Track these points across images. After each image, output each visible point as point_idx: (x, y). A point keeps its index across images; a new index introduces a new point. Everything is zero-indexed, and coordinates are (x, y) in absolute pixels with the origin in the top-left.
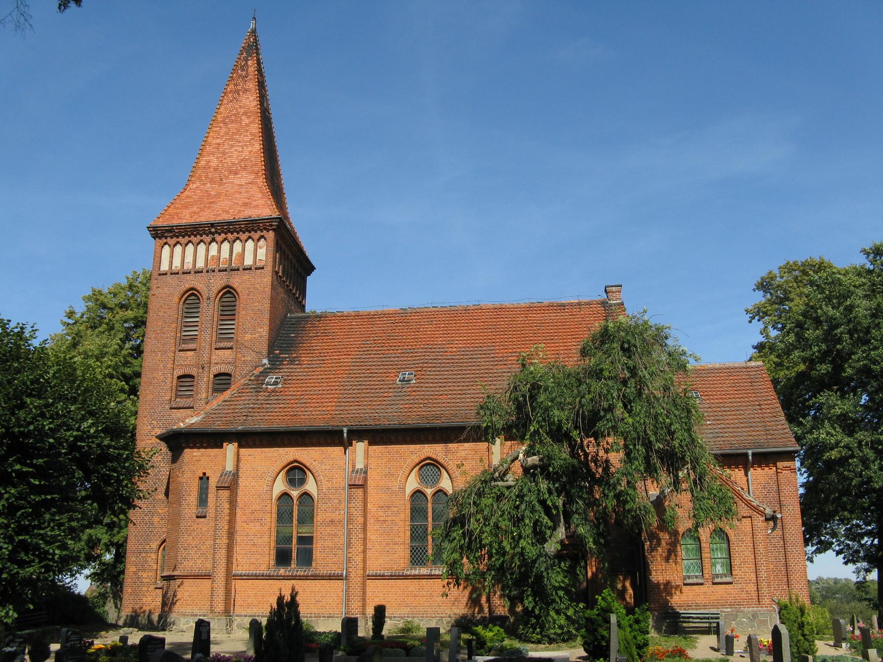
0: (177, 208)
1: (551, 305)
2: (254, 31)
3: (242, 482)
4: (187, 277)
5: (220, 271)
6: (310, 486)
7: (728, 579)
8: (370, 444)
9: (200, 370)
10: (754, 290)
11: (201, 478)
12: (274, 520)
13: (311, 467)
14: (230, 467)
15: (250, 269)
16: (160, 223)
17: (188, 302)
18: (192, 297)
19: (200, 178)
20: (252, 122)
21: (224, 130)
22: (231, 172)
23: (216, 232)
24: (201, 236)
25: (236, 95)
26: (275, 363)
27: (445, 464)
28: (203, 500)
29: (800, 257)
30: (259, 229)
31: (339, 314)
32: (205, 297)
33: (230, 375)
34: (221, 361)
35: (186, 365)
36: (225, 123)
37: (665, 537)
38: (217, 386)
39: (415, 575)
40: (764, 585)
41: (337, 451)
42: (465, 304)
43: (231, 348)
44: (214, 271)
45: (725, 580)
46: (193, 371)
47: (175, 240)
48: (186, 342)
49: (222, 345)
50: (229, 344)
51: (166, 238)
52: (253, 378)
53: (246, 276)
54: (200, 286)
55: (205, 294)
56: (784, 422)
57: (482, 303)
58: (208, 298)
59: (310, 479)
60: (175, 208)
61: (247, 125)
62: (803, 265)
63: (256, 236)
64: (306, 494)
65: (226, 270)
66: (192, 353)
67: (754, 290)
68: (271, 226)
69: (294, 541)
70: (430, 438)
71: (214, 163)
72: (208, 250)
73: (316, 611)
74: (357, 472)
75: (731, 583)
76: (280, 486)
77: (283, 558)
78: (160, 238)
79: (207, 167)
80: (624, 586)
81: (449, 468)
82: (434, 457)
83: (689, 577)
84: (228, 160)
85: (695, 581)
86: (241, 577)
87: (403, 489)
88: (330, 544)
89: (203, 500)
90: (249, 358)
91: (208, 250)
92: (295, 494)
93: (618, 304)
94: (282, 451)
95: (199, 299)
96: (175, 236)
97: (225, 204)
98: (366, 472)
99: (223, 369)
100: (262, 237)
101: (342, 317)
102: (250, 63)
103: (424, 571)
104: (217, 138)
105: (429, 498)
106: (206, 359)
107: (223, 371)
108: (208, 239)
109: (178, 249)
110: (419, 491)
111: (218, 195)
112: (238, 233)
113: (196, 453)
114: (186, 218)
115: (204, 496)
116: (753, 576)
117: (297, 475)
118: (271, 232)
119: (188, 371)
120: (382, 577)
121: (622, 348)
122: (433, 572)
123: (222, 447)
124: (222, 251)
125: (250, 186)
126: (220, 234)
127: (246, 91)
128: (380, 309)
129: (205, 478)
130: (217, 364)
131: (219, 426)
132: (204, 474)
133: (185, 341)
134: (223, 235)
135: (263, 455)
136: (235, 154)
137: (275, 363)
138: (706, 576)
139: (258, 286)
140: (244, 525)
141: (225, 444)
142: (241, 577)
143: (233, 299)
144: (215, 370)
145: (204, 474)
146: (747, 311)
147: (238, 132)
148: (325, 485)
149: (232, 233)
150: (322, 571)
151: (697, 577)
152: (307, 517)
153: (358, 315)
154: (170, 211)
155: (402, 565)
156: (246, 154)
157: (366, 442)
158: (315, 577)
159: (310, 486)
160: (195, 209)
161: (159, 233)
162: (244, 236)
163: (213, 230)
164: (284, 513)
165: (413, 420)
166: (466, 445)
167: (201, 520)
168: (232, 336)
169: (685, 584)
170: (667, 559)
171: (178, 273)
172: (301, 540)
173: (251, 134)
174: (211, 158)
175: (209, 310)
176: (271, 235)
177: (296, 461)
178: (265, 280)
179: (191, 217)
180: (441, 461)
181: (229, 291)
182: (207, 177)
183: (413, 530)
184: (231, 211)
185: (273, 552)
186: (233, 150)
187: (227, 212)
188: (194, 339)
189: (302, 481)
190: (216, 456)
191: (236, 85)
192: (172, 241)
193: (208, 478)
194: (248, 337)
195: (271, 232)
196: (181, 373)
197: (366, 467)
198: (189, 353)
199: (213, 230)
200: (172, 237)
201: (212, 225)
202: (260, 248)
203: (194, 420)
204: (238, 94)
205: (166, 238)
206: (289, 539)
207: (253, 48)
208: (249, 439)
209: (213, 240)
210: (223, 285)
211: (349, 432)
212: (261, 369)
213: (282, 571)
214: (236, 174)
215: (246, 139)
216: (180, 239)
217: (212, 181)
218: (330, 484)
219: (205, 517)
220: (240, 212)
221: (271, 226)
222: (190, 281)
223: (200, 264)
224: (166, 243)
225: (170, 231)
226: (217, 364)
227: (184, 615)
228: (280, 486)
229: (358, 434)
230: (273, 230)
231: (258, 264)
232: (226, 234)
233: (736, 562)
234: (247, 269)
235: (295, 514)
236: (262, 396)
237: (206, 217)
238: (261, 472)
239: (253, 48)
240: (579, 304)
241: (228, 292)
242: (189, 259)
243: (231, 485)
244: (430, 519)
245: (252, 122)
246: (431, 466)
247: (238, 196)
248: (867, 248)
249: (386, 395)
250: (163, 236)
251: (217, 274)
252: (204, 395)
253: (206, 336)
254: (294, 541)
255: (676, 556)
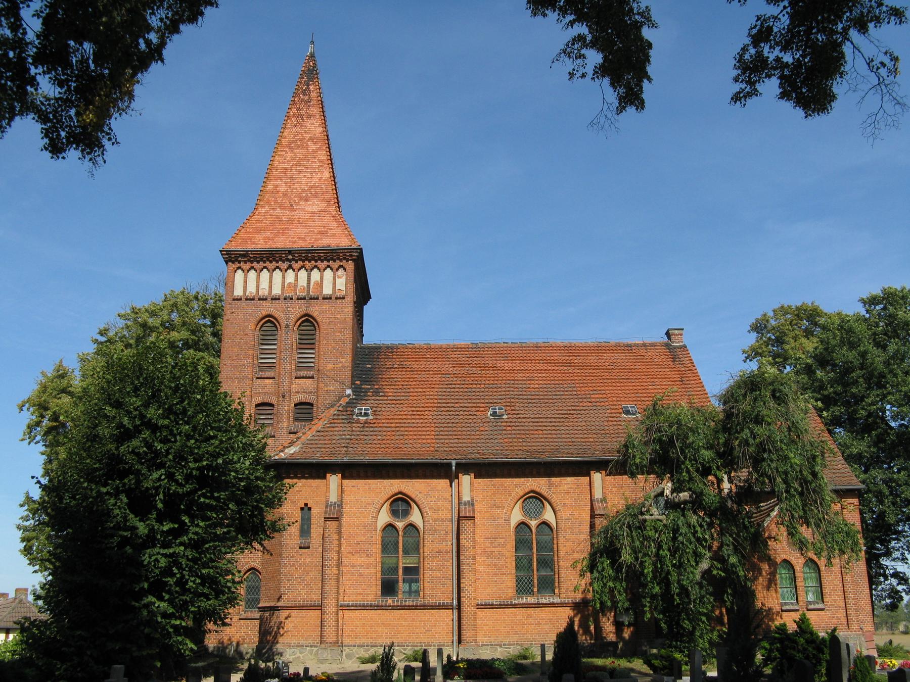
0: (249, 232)
1: (618, 345)
2: (312, 56)
3: (345, 513)
4: (264, 303)
5: (298, 299)
6: (415, 517)
7: (821, 606)
8: (344, 477)
9: (281, 399)
10: (749, 332)
11: (302, 509)
12: (380, 551)
13: (417, 499)
14: (333, 498)
15: (330, 298)
16: (233, 247)
17: (263, 328)
18: (269, 324)
19: (268, 202)
20: (319, 149)
21: (289, 155)
22: (301, 198)
23: (293, 259)
24: (277, 262)
25: (300, 120)
26: (360, 395)
27: (549, 497)
28: (305, 531)
29: (795, 301)
30: (338, 259)
31: (411, 346)
32: (282, 325)
33: (312, 405)
34: (302, 389)
35: (265, 393)
36: (291, 148)
37: (765, 567)
38: (298, 416)
39: (523, 604)
40: (852, 611)
41: (443, 483)
42: (535, 341)
43: (312, 377)
44: (292, 299)
45: (817, 606)
46: (273, 400)
47: (248, 265)
48: (264, 370)
49: (302, 374)
50: (310, 374)
51: (240, 262)
52: (341, 408)
53: (326, 305)
54: (277, 314)
55: (283, 322)
56: (843, 461)
57: (551, 341)
58: (287, 326)
59: (415, 510)
60: (246, 232)
61: (314, 152)
62: (797, 308)
63: (335, 265)
64: (412, 525)
65: (304, 299)
66: (271, 381)
67: (749, 332)
68: (351, 256)
69: (401, 571)
70: (362, 475)
71: (283, 189)
72: (284, 277)
73: (425, 640)
74: (331, 505)
75: (823, 610)
76: (384, 517)
77: (389, 588)
78: (233, 262)
79: (276, 191)
80: (721, 613)
81: (553, 501)
82: (538, 490)
83: (786, 604)
84: (297, 186)
85: (791, 607)
86: (348, 607)
87: (508, 521)
88: (438, 574)
89: (305, 531)
90: (332, 388)
91: (284, 277)
92: (400, 525)
93: (681, 347)
94: (386, 482)
95: (275, 326)
96: (249, 260)
97: (301, 231)
98: (473, 505)
99: (305, 398)
100: (341, 266)
101: (414, 349)
102: (311, 87)
103: (531, 600)
104: (284, 163)
105: (534, 529)
106: (286, 388)
107: (304, 400)
108: (285, 265)
109: (265, 274)
110: (523, 523)
111: (290, 221)
112: (316, 261)
113: (300, 483)
114: (260, 243)
115: (306, 527)
116: (842, 603)
117: (401, 507)
118: (350, 262)
119: (267, 399)
120: (491, 606)
121: (774, 396)
122: (541, 601)
123: (325, 478)
124: (299, 279)
125: (323, 213)
126: (297, 262)
127: (310, 116)
128: (451, 343)
129: (306, 508)
130: (297, 392)
131: (319, 456)
132: (306, 505)
133: (261, 368)
134: (300, 263)
135: (367, 487)
136: (304, 180)
137: (360, 395)
138: (801, 603)
139: (339, 316)
140: (350, 556)
141: (328, 475)
142: (348, 607)
143: (312, 328)
144: (296, 399)
145: (306, 505)
146: (744, 352)
147: (305, 158)
148: (431, 516)
149: (310, 261)
150: (430, 601)
151: (792, 604)
152: (414, 548)
153: (429, 348)
154: (241, 234)
155: (510, 595)
156: (315, 180)
157: (472, 475)
158: (425, 607)
159: (415, 517)
160: (268, 233)
161: (232, 257)
162: (322, 265)
163: (290, 257)
164: (389, 544)
165: (517, 455)
166: (568, 479)
167: (304, 550)
168: (312, 365)
169: (808, 610)
170: (768, 588)
171: (253, 299)
172: (407, 570)
173: (320, 161)
174: (279, 182)
175: (288, 338)
176: (350, 265)
177: (400, 493)
178: (346, 310)
179: (266, 243)
180: (545, 494)
181: (308, 320)
182: (276, 202)
183: (518, 559)
184: (308, 239)
185: (379, 583)
186: (302, 175)
187: (304, 240)
188: (271, 367)
189: (406, 513)
190: (317, 487)
191: (298, 109)
192: (246, 266)
193: (310, 509)
194: (330, 366)
195: (350, 262)
196: (260, 400)
197: (472, 499)
198: (267, 381)
199: (290, 257)
200: (245, 262)
201: (290, 252)
202: (339, 277)
203: (292, 450)
204: (302, 119)
205: (240, 262)
206: (395, 570)
207: (311, 73)
208: (352, 470)
209: (290, 267)
210: (302, 313)
211: (457, 464)
212: (347, 400)
213: (390, 601)
214: (307, 200)
215: (314, 165)
216: (255, 264)
217: (281, 206)
218: (436, 516)
219: (308, 548)
220: (316, 240)
221: (351, 256)
222: (267, 308)
223: (277, 291)
224: (239, 268)
225: (244, 256)
226: (297, 392)
227: (290, 646)
228: (384, 517)
229: (465, 467)
230: (353, 260)
231: (338, 294)
232: (303, 261)
233: (826, 590)
234: (327, 298)
235: (401, 545)
236: (356, 427)
237: (281, 243)
238: (366, 504)
239: (311, 73)
240: (644, 345)
241: (307, 321)
242: (264, 285)
243: (334, 516)
244: (535, 550)
245: (319, 149)
246: (536, 499)
247: (312, 224)
248: (865, 297)
249: (482, 429)
250: (236, 260)
251: (295, 301)
252: (285, 425)
253: (287, 362)
254: (401, 571)
255: (776, 585)
